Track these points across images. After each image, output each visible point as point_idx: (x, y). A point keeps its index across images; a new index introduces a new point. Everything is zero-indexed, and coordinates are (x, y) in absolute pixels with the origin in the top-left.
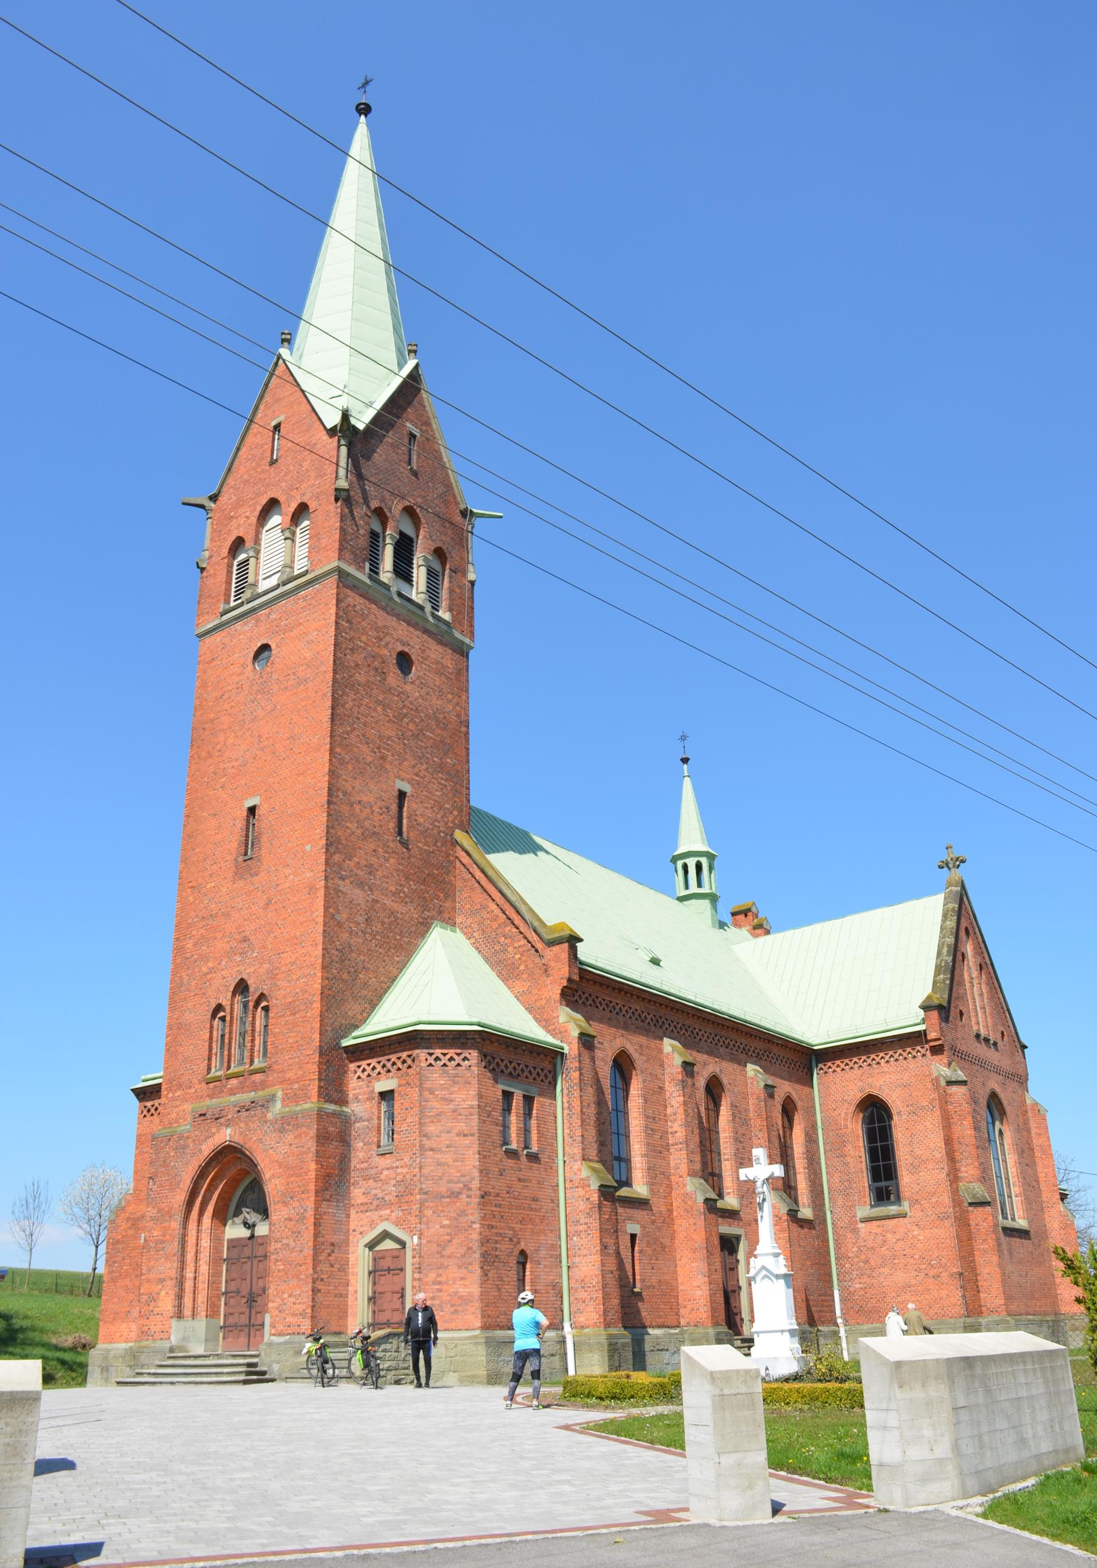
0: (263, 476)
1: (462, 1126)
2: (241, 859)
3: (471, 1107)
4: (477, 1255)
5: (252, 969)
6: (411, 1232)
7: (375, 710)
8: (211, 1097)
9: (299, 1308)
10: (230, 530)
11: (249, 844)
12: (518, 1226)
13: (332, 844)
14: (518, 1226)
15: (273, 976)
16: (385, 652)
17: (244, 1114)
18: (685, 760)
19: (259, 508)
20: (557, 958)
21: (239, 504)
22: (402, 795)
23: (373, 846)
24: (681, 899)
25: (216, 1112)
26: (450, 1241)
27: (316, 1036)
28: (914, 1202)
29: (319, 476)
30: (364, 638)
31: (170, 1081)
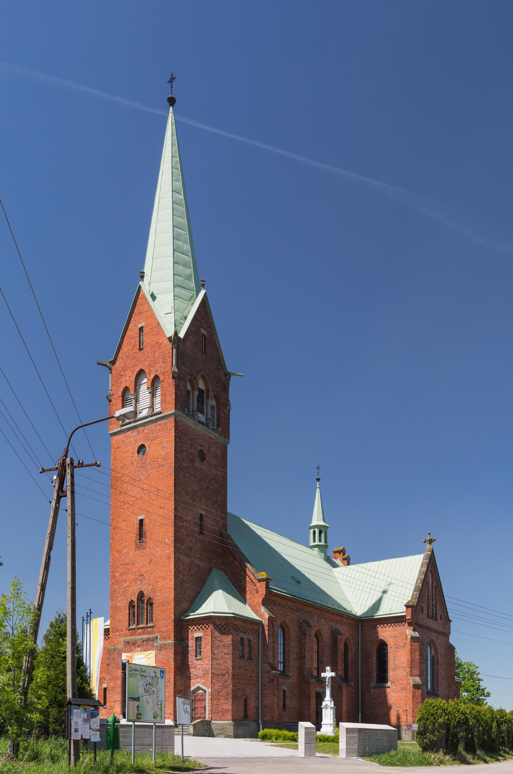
0: (137, 355)
1: (226, 651)
2: (138, 541)
3: (229, 644)
4: (231, 696)
5: (145, 587)
6: (208, 687)
8: (131, 636)
9: (169, 712)
11: (141, 535)
14: (244, 686)
15: (154, 590)
16: (194, 451)
17: (145, 643)
18: (318, 480)
19: (135, 373)
20: (261, 587)
21: (125, 368)
22: (201, 516)
23: (191, 539)
24: (312, 547)
25: (134, 641)
26: (222, 691)
27: (173, 616)
28: (393, 682)
30: (186, 446)
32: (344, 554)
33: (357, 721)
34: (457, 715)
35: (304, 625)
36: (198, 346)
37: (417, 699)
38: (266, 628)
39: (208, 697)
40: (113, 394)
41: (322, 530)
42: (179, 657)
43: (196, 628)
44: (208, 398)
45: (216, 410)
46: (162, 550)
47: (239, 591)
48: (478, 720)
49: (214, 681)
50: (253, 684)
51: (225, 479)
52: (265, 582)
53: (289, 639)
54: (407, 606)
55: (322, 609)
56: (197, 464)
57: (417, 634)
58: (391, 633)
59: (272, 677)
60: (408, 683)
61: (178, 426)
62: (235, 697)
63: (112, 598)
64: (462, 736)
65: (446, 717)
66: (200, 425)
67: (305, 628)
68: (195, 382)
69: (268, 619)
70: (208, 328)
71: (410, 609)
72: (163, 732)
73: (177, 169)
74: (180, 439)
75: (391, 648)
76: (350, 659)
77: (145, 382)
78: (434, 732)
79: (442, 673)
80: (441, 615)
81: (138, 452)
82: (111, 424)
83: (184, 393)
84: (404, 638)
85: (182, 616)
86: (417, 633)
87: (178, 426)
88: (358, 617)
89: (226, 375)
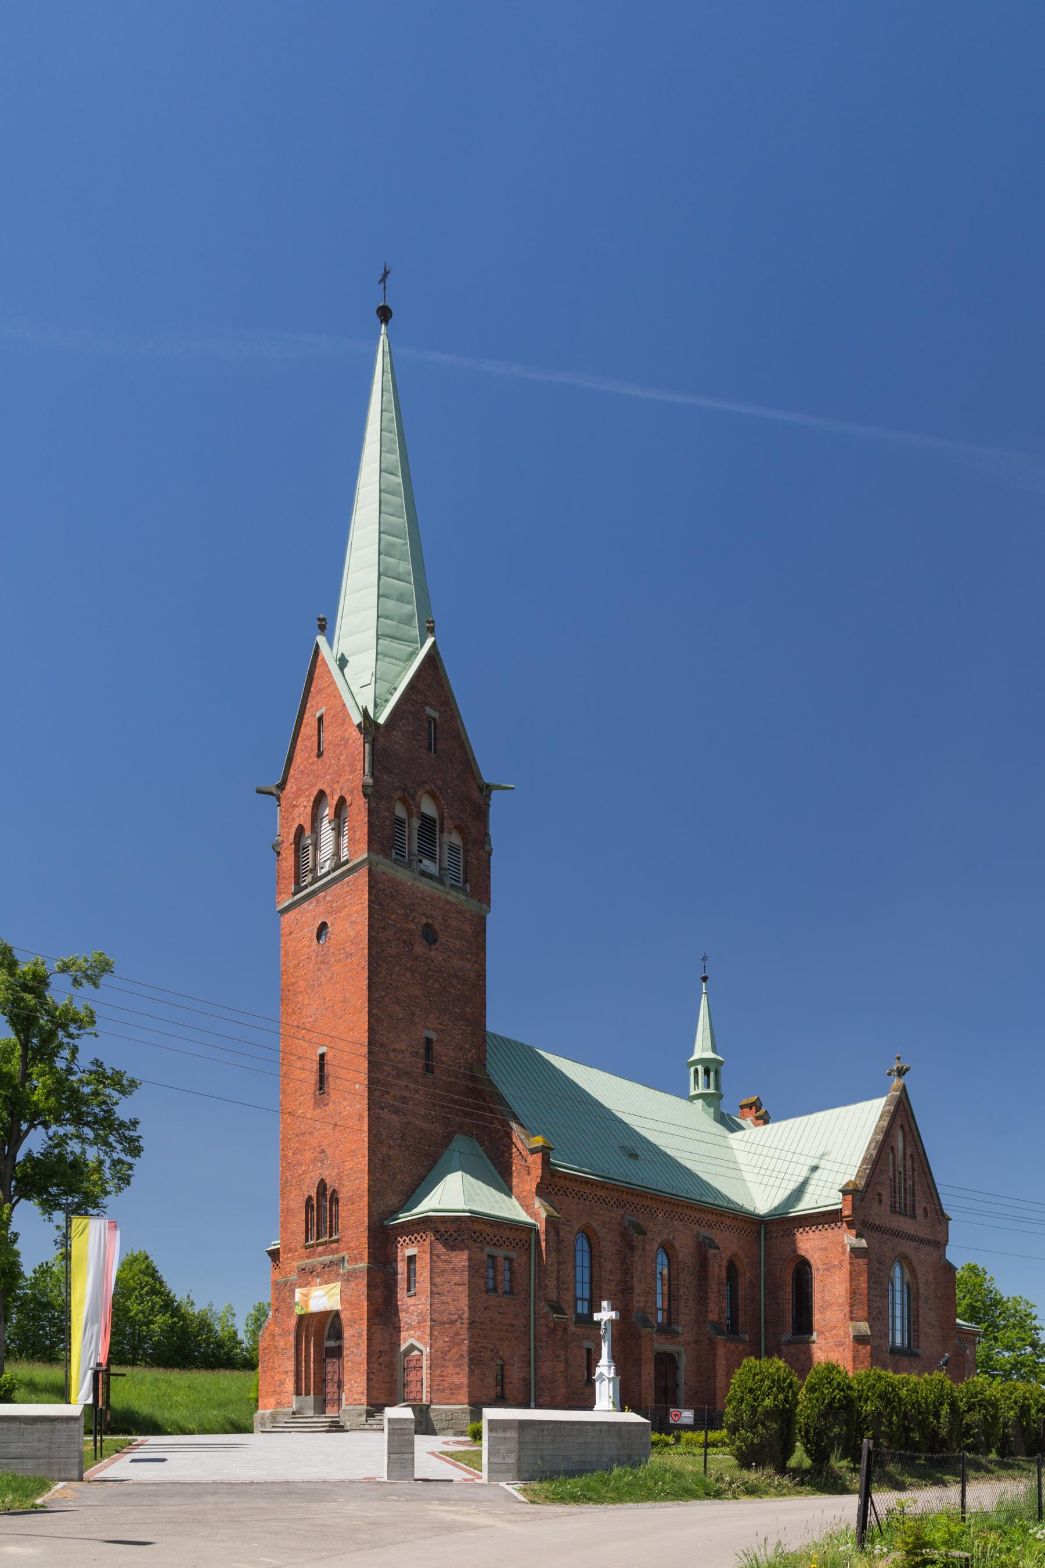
0: (314, 767)
1: (457, 1279)
2: (317, 1093)
3: (464, 1266)
7: (405, 975)
8: (308, 1258)
9: (360, 1389)
10: (294, 819)
11: (322, 1080)
12: (497, 1343)
13: (372, 1082)
14: (497, 1343)
16: (412, 926)
18: (705, 979)
22: (429, 1041)
29: (352, 771)
30: (393, 917)
31: (284, 1247)
32: (758, 1109)
33: (526, 1405)
34: (826, 1392)
35: (631, 1231)
36: (419, 738)
37: (862, 1363)
38: (543, 1237)
39: (425, 1363)
40: (283, 842)
41: (709, 1068)
42: (378, 1293)
43: (407, 1241)
44: (442, 831)
45: (461, 852)
46: (351, 1105)
47: (500, 1173)
48: (889, 1402)
49: (436, 1333)
50: (516, 1338)
51: (481, 975)
52: (540, 1154)
53: (600, 1256)
54: (844, 1192)
55: (673, 1201)
56: (419, 949)
57: (863, 1243)
58: (817, 1243)
59: (551, 1325)
60: (847, 1334)
61: (377, 883)
62: (475, 1362)
63: (283, 1195)
64: (838, 1436)
65: (781, 1396)
66: (424, 879)
67: (632, 1236)
68: (411, 802)
69: (547, 1220)
70: (442, 705)
71: (849, 1197)
72: (53, 1431)
73: (390, 432)
74: (380, 904)
75: (818, 1269)
76: (741, 1293)
77: (328, 811)
78: (755, 1426)
79: (928, 1314)
80: (925, 1209)
81: (319, 937)
82: (280, 893)
83: (388, 822)
84: (840, 1250)
85: (386, 1219)
86: (864, 1241)
87: (377, 883)
88: (758, 1215)
89: (481, 790)
